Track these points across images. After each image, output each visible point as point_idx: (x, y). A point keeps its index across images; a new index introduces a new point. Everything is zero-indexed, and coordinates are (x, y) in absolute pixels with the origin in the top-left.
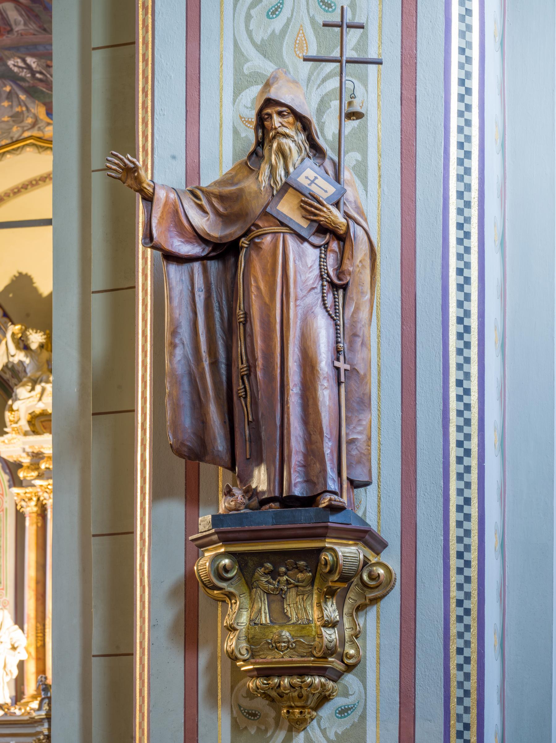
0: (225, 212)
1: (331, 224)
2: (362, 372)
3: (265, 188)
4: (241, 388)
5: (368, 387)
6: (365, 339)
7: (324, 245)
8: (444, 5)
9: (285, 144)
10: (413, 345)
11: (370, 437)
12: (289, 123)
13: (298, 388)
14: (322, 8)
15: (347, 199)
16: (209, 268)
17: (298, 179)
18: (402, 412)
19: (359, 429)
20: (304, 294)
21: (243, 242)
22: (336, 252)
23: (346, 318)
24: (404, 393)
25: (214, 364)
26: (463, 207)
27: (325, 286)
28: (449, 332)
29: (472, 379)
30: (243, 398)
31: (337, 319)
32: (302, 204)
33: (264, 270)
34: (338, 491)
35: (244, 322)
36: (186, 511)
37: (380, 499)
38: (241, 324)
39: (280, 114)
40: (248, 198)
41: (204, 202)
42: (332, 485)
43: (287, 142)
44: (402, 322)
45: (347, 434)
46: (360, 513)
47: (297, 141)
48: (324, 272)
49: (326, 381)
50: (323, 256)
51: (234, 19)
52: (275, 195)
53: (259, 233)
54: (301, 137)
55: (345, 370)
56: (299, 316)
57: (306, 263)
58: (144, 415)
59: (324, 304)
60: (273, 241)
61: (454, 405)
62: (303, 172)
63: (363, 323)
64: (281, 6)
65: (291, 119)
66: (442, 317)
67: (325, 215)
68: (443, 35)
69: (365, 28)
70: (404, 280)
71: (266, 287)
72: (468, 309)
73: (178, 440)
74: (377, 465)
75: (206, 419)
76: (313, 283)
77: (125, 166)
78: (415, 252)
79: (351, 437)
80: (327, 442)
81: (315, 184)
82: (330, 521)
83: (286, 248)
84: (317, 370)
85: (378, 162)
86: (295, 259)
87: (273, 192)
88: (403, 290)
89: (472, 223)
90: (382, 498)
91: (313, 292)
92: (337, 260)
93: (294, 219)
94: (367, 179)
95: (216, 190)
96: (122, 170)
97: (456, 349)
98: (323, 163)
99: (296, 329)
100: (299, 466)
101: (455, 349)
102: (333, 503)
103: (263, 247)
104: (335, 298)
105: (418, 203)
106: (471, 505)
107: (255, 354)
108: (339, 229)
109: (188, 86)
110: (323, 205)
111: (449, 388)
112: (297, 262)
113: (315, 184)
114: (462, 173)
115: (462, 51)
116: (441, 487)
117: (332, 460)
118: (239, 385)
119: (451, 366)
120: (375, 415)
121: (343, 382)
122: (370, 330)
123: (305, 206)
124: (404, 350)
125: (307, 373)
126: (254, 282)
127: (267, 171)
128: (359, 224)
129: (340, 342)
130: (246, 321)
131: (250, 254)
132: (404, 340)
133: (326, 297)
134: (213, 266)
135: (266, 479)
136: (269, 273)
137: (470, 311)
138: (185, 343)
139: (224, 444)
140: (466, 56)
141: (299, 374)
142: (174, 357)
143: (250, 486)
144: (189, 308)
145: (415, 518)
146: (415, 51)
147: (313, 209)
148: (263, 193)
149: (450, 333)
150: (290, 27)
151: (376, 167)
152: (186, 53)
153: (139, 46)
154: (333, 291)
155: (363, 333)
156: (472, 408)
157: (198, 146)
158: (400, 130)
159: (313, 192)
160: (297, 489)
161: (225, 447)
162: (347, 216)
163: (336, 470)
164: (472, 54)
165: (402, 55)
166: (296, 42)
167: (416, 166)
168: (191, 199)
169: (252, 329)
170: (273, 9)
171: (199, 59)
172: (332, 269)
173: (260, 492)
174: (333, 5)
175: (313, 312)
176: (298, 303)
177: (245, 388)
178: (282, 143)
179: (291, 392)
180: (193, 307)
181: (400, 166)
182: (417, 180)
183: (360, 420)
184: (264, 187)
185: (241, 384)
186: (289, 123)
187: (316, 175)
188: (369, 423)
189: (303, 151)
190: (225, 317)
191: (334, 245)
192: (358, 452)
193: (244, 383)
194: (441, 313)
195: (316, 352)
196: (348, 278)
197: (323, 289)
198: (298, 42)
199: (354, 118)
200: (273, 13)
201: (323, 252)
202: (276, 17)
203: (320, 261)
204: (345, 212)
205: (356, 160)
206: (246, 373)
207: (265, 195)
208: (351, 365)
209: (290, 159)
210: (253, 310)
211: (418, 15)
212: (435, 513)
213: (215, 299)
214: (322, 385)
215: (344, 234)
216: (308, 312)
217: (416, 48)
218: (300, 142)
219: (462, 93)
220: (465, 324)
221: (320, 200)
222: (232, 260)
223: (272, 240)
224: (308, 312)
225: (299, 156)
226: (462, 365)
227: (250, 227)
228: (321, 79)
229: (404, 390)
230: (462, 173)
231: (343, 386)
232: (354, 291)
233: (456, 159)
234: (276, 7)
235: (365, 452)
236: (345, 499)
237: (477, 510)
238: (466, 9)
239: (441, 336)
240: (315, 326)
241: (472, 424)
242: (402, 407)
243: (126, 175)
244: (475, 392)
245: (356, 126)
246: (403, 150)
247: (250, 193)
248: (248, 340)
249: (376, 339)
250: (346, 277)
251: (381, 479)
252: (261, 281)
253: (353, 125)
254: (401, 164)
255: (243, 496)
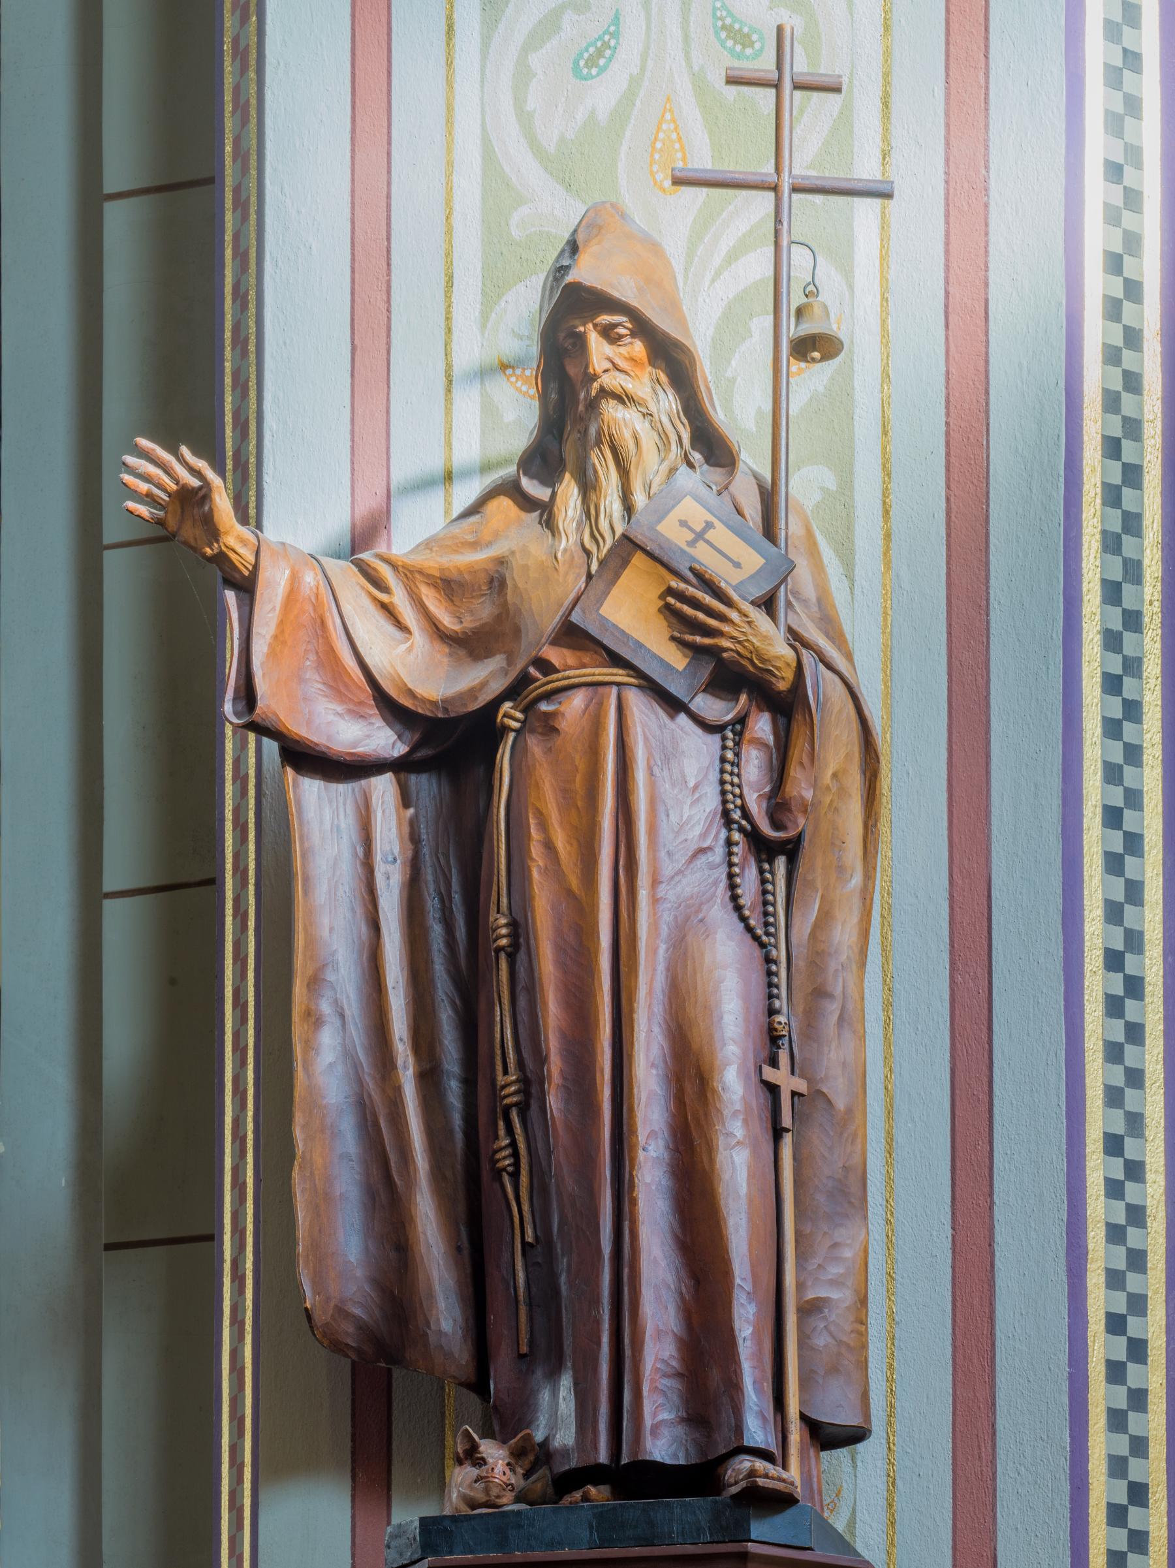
0: (457, 628)
1: (751, 661)
2: (840, 1104)
3: (568, 554)
4: (503, 1144)
5: (860, 1146)
6: (850, 1006)
7: (733, 723)
8: (1063, 37)
9: (622, 423)
10: (985, 1030)
11: (866, 1297)
12: (632, 360)
13: (661, 1143)
14: (725, 48)
15: (796, 594)
16: (414, 795)
17: (659, 528)
18: (953, 1229)
19: (835, 1270)
20: (679, 866)
21: (506, 715)
22: (766, 745)
23: (794, 940)
24: (958, 1172)
25: (429, 1077)
26: (1121, 629)
27: (737, 844)
28: (1083, 994)
29: (1149, 1133)
30: (508, 1173)
31: (770, 944)
32: (671, 600)
33: (565, 793)
34: (774, 1448)
35: (509, 949)
36: (353, 1517)
37: (894, 1484)
38: (503, 956)
39: (608, 333)
40: (520, 585)
41: (399, 599)
42: (757, 1432)
43: (628, 416)
44: (952, 963)
45: (800, 1286)
46: (840, 1525)
47: (656, 415)
48: (733, 803)
49: (739, 1124)
50: (730, 755)
51: (482, 82)
52: (593, 572)
53: (549, 687)
54: (667, 403)
55: (794, 1094)
56: (664, 931)
57: (683, 776)
58: (237, 1235)
59: (735, 898)
60: (591, 708)
61: (1097, 1208)
62: (674, 507)
63: (843, 958)
64: (613, 43)
65: (638, 348)
66: (1065, 949)
67: (735, 634)
68: (1061, 125)
69: (844, 87)
70: (956, 840)
71: (571, 845)
72: (1136, 927)
73: (328, 1300)
74: (884, 1384)
75: (407, 1240)
76: (704, 835)
77: (177, 484)
78: (988, 756)
79: (810, 1295)
80: (742, 1305)
81: (707, 542)
82: (753, 1537)
83: (627, 729)
84: (714, 1091)
85: (884, 495)
86: (652, 762)
87: (589, 567)
88: (955, 870)
89: (1145, 674)
90: (899, 1482)
91: (702, 860)
92: (771, 769)
93: (648, 645)
94: (853, 543)
95: (434, 562)
96: (169, 497)
97: (1104, 1045)
98: (729, 483)
99: (654, 970)
100: (665, 1375)
101: (1101, 1043)
102: (761, 1481)
103: (563, 725)
104: (764, 881)
105: (994, 616)
106: (1147, 1507)
107: (540, 1045)
108: (774, 676)
109: (357, 276)
110: (728, 602)
111: (1085, 1157)
112: (656, 770)
113: (707, 542)
114: (1118, 714)
115: (1114, 171)
116: (1065, 1448)
117: (757, 1356)
118: (496, 1137)
119: (1089, 1093)
120: (877, 1237)
121: (787, 1130)
122: (862, 980)
123: (679, 605)
124: (958, 1045)
125: (687, 1101)
126: (538, 830)
127: (572, 504)
128: (829, 667)
129: (778, 1012)
130: (515, 945)
131: (525, 749)
132: (957, 1018)
133: (738, 875)
134: (424, 784)
135: (573, 1414)
136: (579, 804)
137: (1141, 933)
138: (348, 1013)
139: (457, 1313)
140: (1125, 188)
141: (663, 1102)
142: (317, 1054)
143: (528, 1438)
144: (359, 911)
145: (991, 1540)
146: (983, 171)
147: (701, 616)
148: (562, 569)
149: (1086, 997)
150: (638, 103)
151: (877, 463)
152: (353, 180)
153: (224, 165)
154: (759, 862)
155: (844, 987)
156: (1149, 1220)
157: (384, 450)
158: (943, 402)
159: (701, 564)
160: (659, 1443)
161: (460, 1320)
162: (796, 638)
163: (768, 1387)
164: (1141, 183)
165: (947, 182)
166: (654, 148)
167: (988, 506)
168: (363, 588)
169: (531, 970)
170: (592, 50)
171: (389, 196)
172: (755, 795)
173: (556, 1450)
174: (755, 37)
175: (701, 921)
176: (662, 890)
177: (513, 1144)
178: (614, 419)
179: (641, 1155)
180: (370, 907)
181: (944, 505)
182: (991, 546)
183: (835, 1245)
184: (565, 550)
185: (502, 1132)
186: (632, 360)
187: (711, 518)
188: (862, 1254)
189: (674, 447)
190: (459, 940)
191: (762, 726)
192: (830, 1340)
193: (510, 1131)
194: (1061, 937)
195: (711, 1037)
196: (801, 821)
197: (730, 854)
198: (659, 145)
199: (816, 355)
200: (591, 62)
201: (730, 744)
202: (598, 75)
203: (722, 771)
204: (790, 630)
205: (822, 489)
206: (515, 1099)
207: (566, 574)
208: (810, 1081)
209: (637, 468)
210: (533, 911)
211: (992, 65)
212: (1049, 1526)
213: (432, 887)
214: (729, 1135)
215: (789, 691)
216: (687, 919)
217: (987, 162)
218: (665, 420)
219: (1119, 1085)
220: (1127, 972)
221: (720, 588)
222: (481, 771)
223: (587, 707)
224: (687, 919)
225: (663, 460)
226: (1120, 1091)
227: (527, 667)
228: (723, 254)
229: (958, 1164)
230: (1118, 714)
231: (787, 1139)
232: (819, 863)
233: (1099, 484)
234: (599, 44)
235: (851, 1340)
236: (794, 1473)
237: (1165, 1519)
238: (1125, 50)
239: (1062, 1003)
240: (707, 960)
241: (1149, 1265)
242: (953, 1214)
243: (179, 511)
244: (1156, 1172)
245: (821, 389)
246: (953, 460)
247: (526, 568)
248: (522, 1002)
249: (881, 1014)
250: (796, 818)
251: (896, 1426)
252: (557, 826)
253: (812, 388)
254: (948, 500)
255: (508, 1464)
